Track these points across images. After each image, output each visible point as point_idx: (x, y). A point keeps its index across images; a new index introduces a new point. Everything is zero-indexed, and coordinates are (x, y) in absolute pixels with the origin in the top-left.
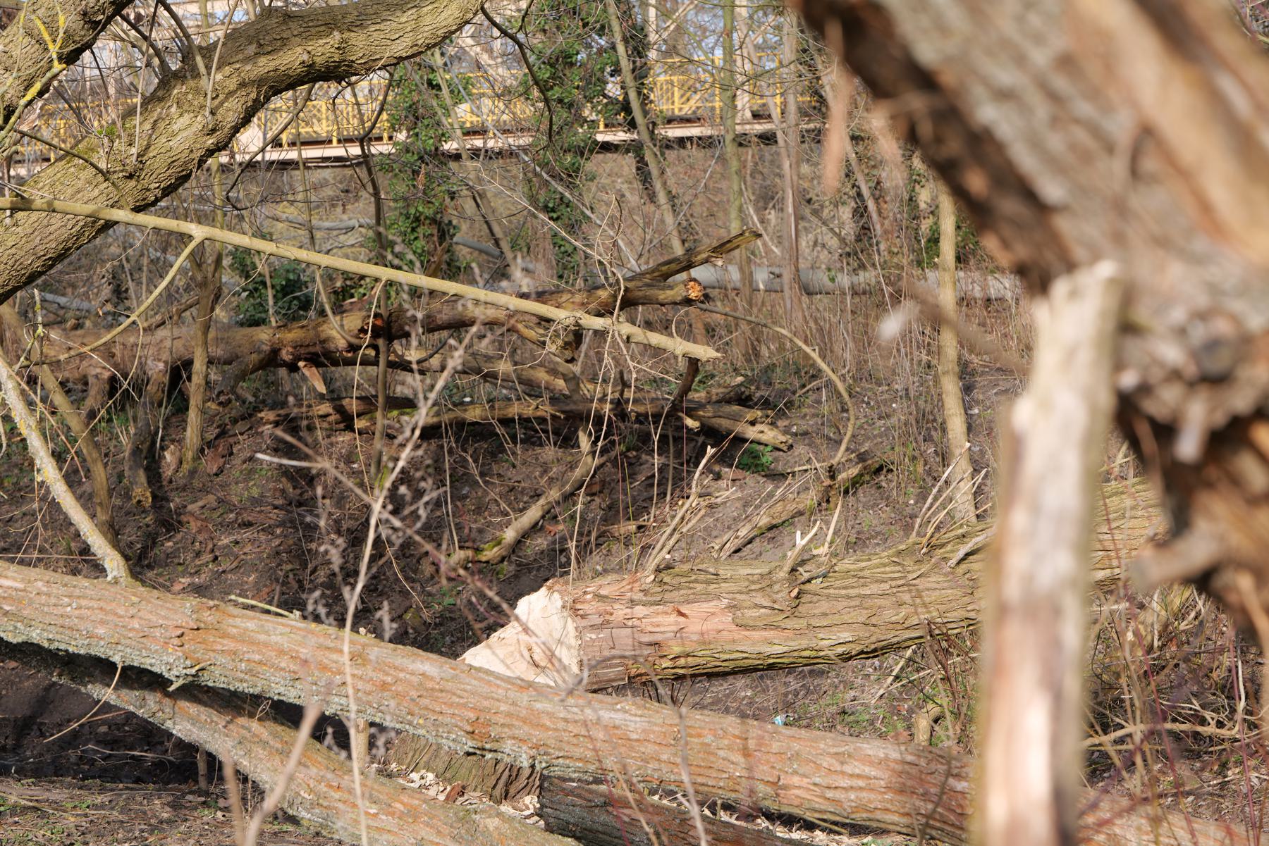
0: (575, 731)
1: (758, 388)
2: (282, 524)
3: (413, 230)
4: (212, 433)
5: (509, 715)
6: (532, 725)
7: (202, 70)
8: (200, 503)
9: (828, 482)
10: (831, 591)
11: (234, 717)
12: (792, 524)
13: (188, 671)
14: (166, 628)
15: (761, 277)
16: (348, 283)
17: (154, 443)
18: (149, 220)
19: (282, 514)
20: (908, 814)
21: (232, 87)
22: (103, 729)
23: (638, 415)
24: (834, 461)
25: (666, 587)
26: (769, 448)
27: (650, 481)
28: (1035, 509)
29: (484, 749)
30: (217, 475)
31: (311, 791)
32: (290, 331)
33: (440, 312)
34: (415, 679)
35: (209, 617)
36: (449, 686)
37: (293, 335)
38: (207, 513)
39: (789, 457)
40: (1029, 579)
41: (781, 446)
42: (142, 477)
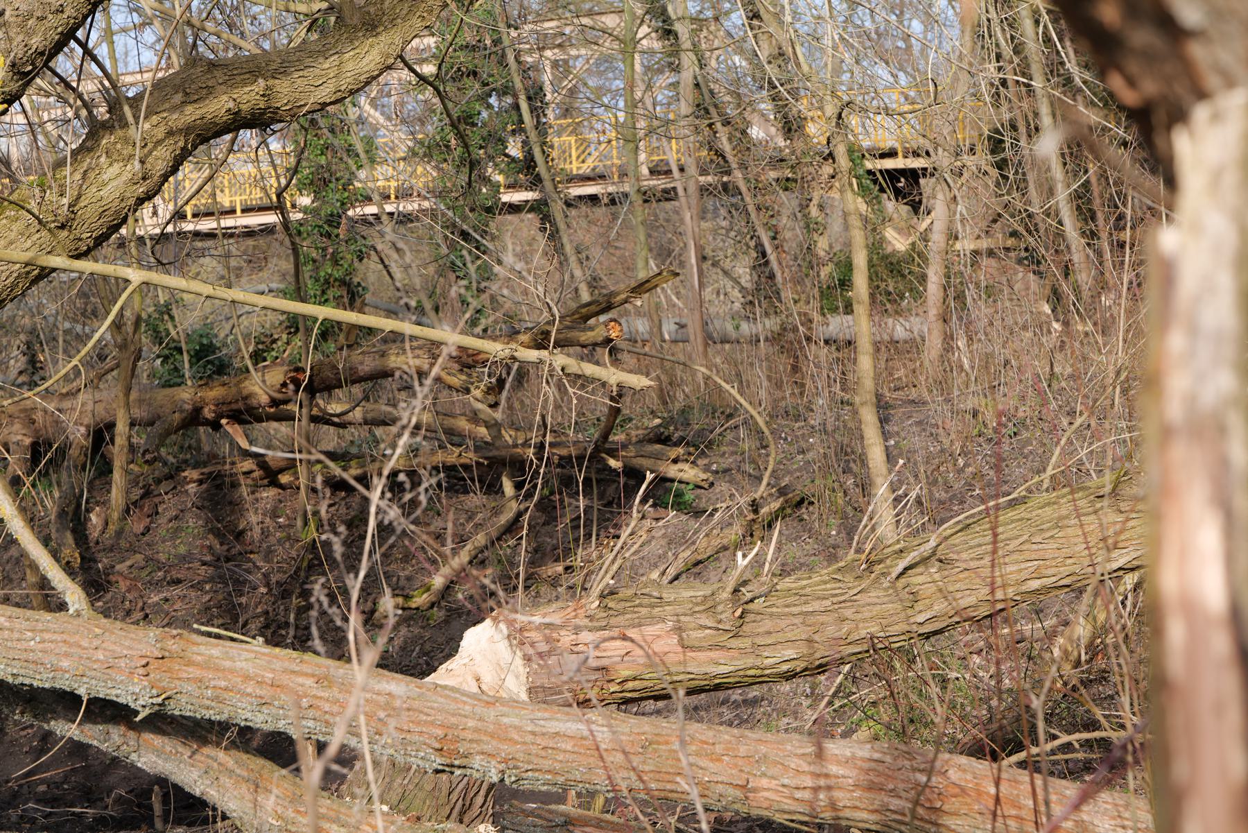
0: (544, 744)
1: (676, 429)
2: (211, 580)
3: (323, 292)
4: (137, 493)
5: (476, 730)
6: (500, 739)
7: (130, 119)
8: (128, 563)
9: (751, 516)
10: (774, 610)
11: (200, 747)
12: (717, 559)
13: (155, 701)
14: (131, 658)
15: (668, 329)
16: (260, 347)
17: (79, 505)
18: (86, 266)
19: (211, 570)
20: (876, 811)
21: (160, 136)
22: (42, 788)
23: (561, 458)
24: (757, 496)
25: (611, 612)
26: (691, 487)
27: (575, 523)
28: (1193, 330)
29: (453, 766)
30: (143, 534)
31: (280, 817)
32: (211, 389)
33: (362, 363)
34: (382, 699)
35: (173, 646)
36: (416, 704)
37: (215, 393)
38: (135, 572)
39: (710, 494)
40: (1191, 401)
41: (702, 484)
42: (69, 538)
